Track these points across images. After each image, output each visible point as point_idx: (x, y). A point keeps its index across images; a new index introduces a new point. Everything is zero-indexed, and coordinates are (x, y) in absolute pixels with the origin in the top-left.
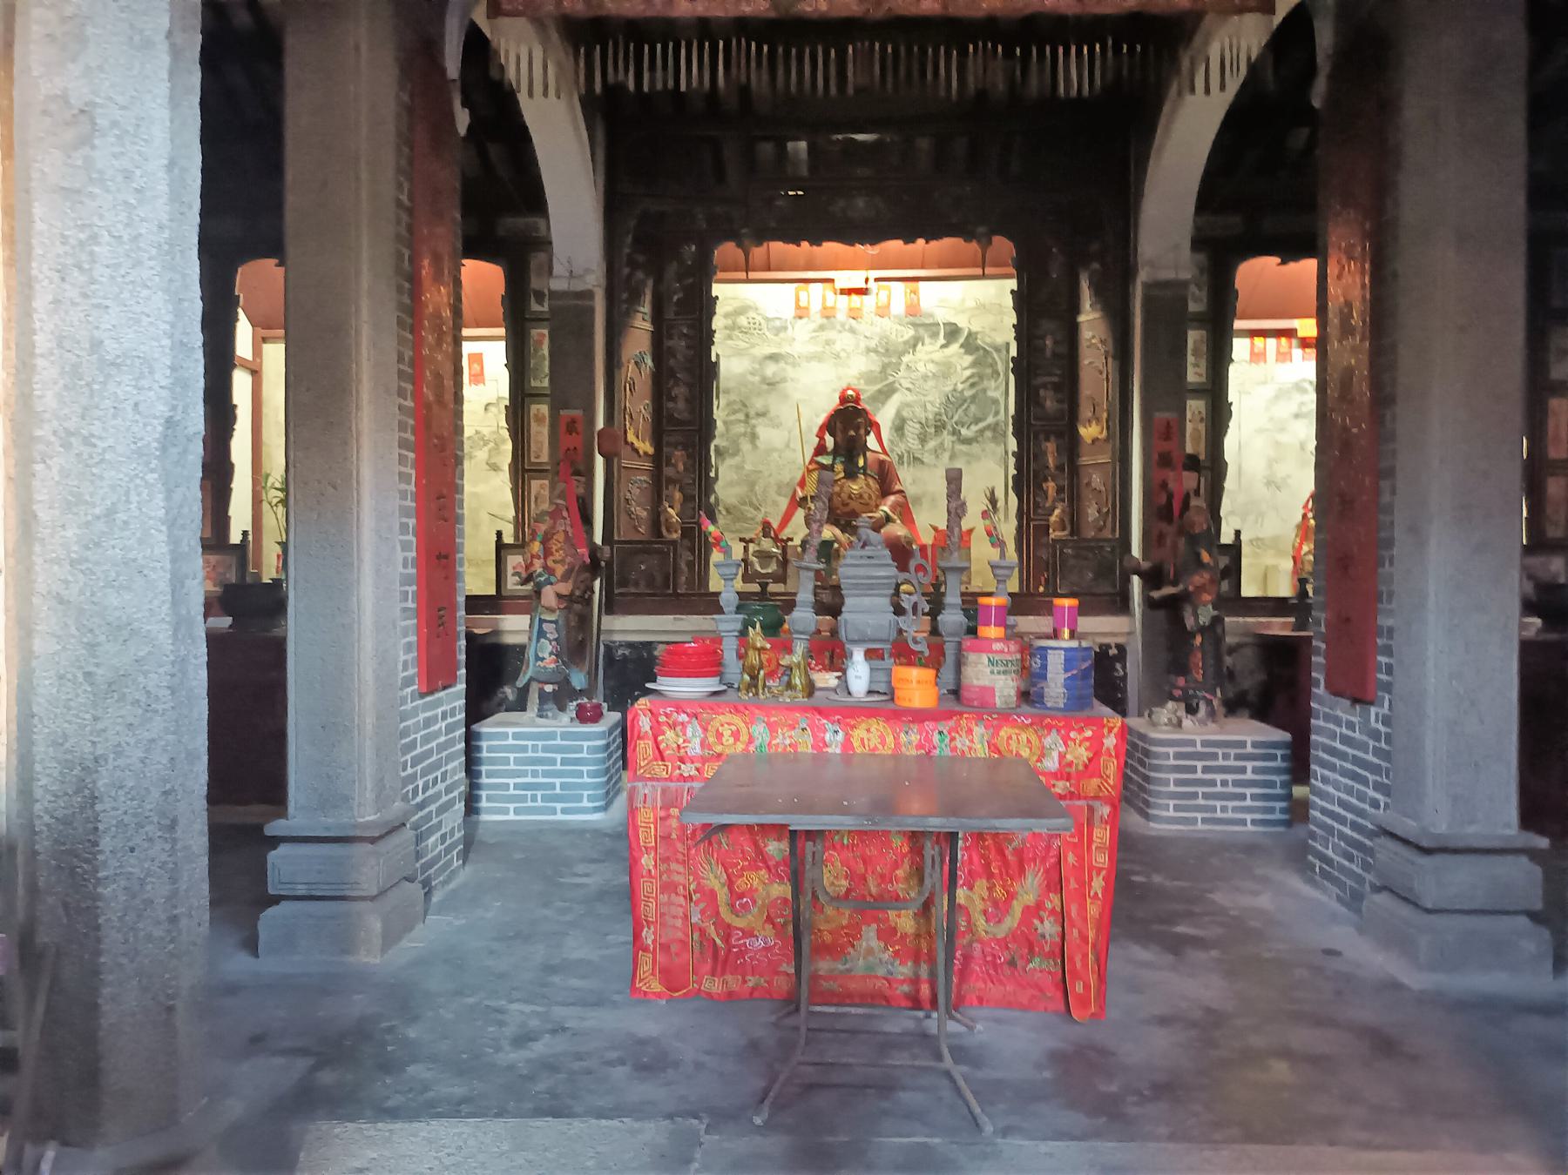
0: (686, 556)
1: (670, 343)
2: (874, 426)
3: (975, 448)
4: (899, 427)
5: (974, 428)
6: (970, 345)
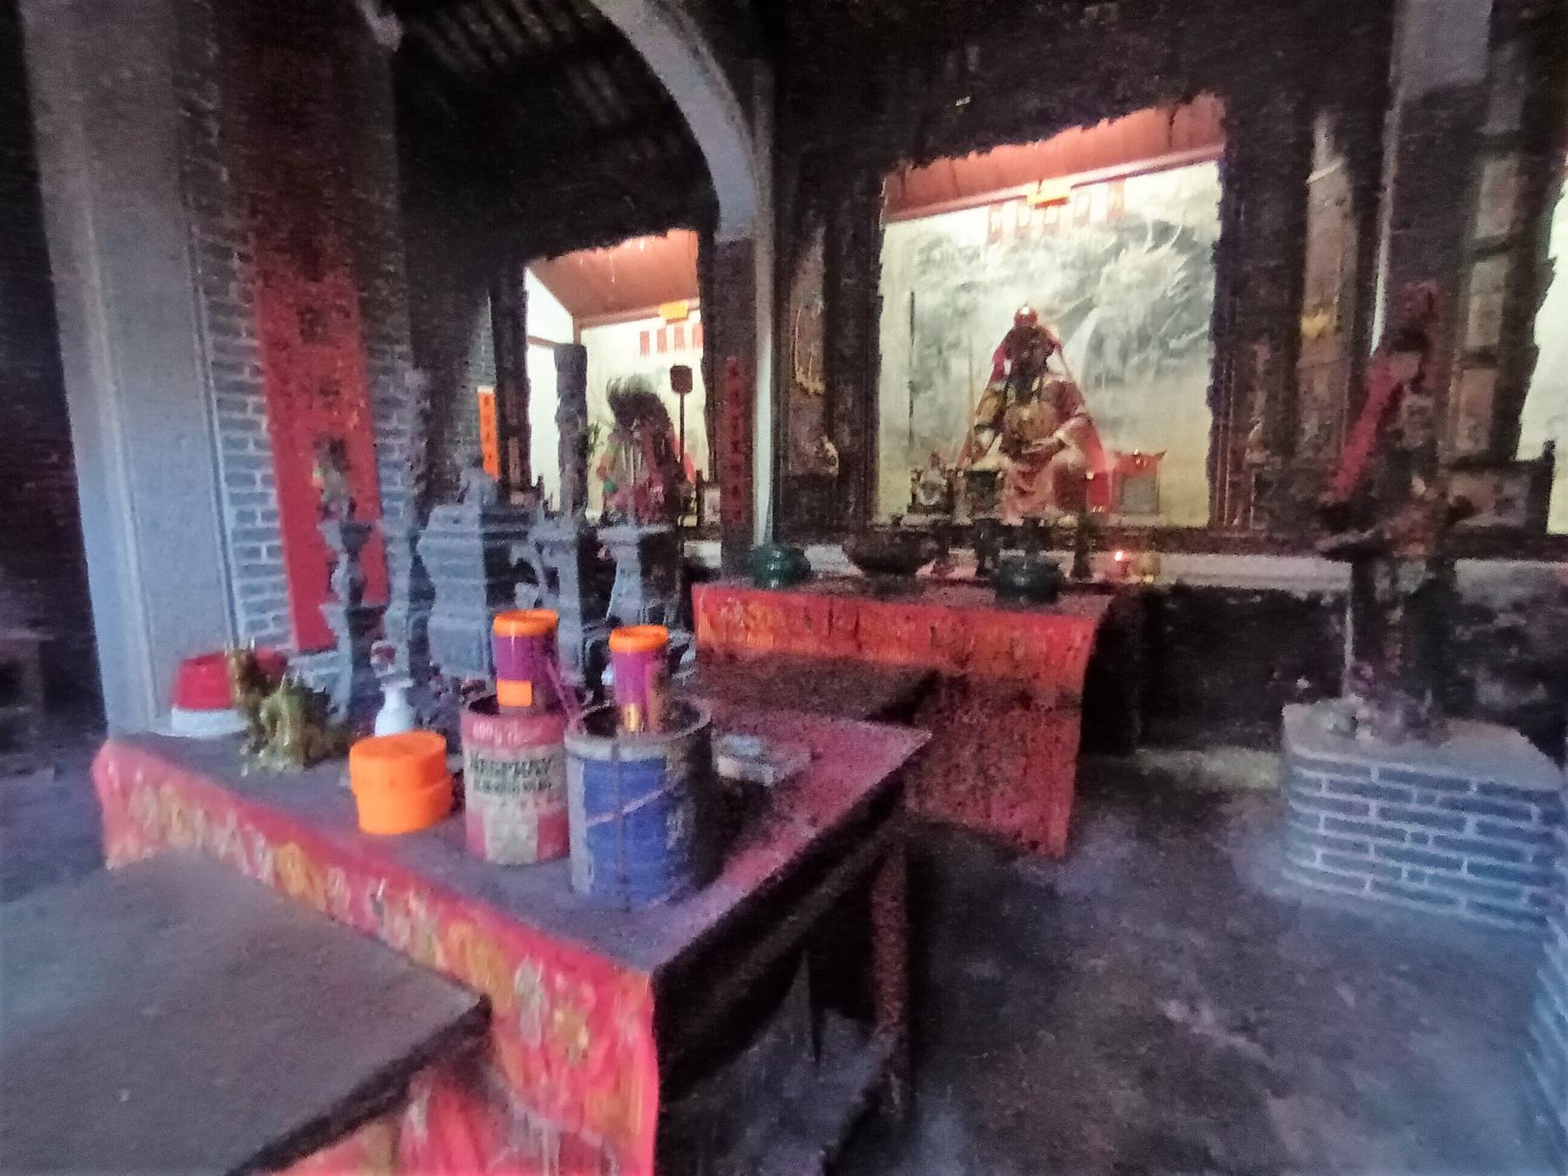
5: (1186, 338)
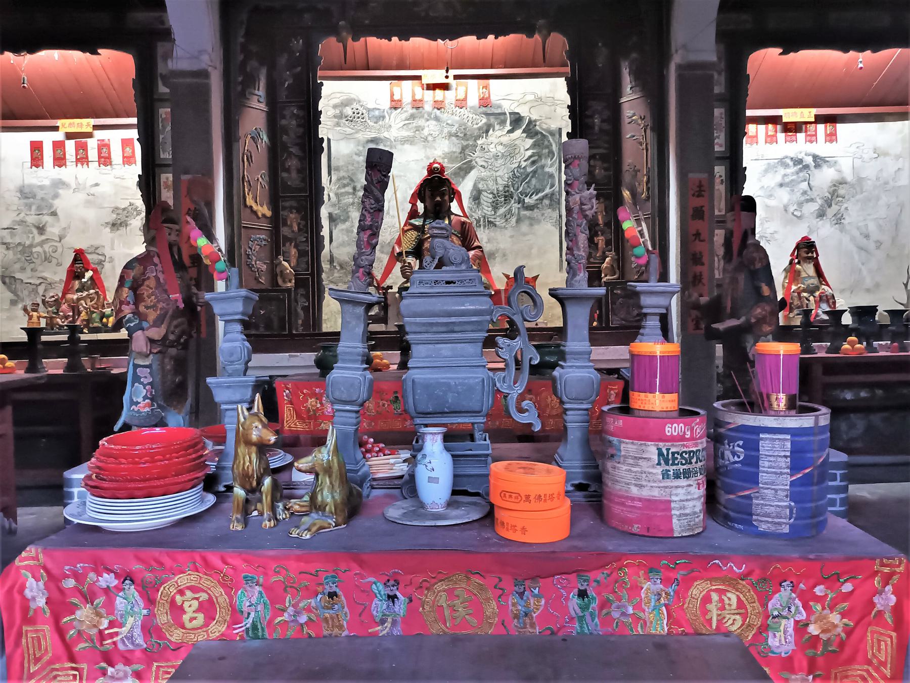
0: (302, 302)
1: (284, 122)
2: (455, 194)
3: (536, 213)
4: (476, 197)
5: (535, 197)
6: (531, 130)
